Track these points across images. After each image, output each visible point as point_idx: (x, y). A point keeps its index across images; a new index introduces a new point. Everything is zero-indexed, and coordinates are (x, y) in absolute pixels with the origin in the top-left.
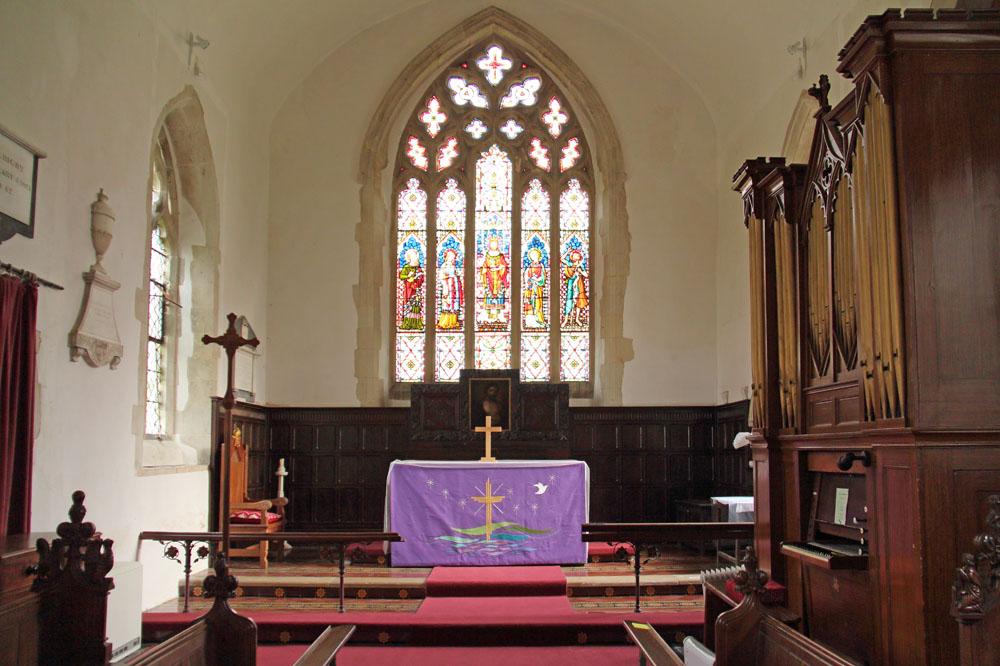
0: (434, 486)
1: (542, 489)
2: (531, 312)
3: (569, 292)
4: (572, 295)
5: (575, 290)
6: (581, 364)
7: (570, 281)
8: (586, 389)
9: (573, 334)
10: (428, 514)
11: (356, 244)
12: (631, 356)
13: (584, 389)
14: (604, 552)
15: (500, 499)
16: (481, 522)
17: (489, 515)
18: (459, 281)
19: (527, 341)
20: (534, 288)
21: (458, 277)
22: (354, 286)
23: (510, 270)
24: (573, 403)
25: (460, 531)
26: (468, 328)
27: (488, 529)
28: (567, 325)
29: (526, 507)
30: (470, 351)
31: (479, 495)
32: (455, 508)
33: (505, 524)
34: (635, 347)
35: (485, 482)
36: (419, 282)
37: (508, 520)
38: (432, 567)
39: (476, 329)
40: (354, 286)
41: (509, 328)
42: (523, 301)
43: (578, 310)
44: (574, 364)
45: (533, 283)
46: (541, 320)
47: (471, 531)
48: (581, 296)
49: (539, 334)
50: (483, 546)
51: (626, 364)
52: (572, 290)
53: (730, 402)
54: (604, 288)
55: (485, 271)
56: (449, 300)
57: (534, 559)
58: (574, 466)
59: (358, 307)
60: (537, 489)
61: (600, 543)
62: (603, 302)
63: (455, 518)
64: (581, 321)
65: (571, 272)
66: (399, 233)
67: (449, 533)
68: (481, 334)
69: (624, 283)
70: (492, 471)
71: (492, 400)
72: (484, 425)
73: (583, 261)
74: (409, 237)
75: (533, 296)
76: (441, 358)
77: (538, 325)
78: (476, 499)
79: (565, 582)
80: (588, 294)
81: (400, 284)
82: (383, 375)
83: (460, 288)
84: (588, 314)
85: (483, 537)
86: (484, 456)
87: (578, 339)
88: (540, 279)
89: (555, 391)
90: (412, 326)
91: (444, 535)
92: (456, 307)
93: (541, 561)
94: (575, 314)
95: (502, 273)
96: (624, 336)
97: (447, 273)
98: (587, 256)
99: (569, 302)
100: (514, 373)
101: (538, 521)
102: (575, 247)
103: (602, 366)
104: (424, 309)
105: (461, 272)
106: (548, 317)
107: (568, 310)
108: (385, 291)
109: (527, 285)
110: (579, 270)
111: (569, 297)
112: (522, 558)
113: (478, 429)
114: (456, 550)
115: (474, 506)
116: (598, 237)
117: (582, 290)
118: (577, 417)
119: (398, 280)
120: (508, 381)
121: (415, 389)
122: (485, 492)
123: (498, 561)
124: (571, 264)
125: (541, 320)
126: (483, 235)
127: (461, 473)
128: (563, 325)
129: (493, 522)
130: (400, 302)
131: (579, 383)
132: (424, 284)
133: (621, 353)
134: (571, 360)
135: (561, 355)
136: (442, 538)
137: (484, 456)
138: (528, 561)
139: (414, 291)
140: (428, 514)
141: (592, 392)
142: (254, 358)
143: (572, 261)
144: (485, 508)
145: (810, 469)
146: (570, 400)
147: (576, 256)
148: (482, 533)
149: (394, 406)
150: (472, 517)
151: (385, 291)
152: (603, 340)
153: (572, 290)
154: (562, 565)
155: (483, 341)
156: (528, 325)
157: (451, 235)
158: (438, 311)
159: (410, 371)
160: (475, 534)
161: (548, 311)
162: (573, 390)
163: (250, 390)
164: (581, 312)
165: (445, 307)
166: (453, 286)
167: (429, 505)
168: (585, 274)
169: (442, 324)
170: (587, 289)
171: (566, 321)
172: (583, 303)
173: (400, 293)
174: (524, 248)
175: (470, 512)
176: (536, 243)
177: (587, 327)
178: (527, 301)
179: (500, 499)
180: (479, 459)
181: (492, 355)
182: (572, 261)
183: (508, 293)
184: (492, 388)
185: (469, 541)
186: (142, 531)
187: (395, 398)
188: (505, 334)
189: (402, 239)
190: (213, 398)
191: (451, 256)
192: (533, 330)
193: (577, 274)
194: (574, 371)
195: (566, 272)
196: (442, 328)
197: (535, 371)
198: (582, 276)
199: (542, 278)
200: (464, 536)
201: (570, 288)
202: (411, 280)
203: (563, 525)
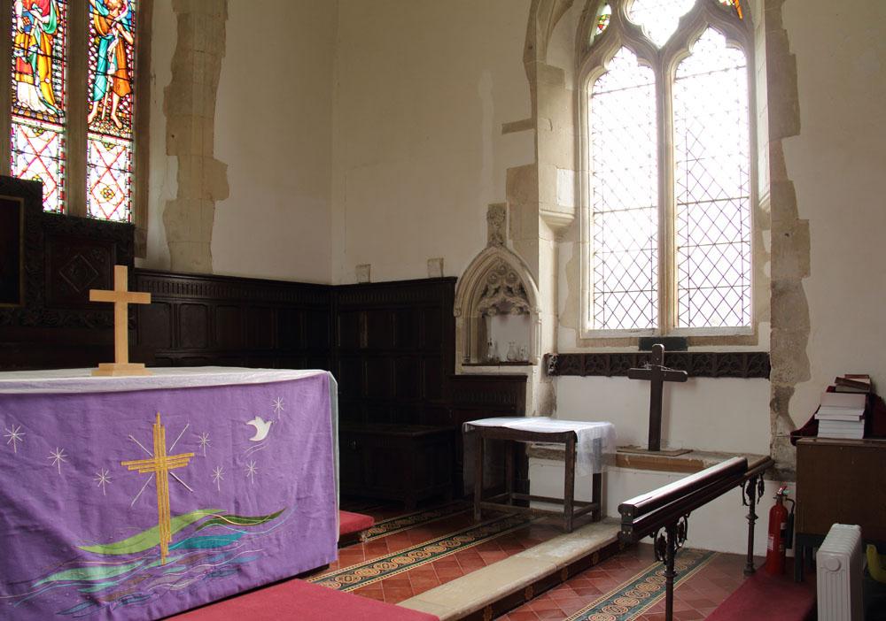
0: (25, 445)
1: (262, 429)
3: (101, 60)
4: (107, 68)
5: (112, 60)
6: (119, 196)
7: (104, 42)
9: (107, 139)
10: (12, 521)
12: (225, 194)
15: (184, 459)
16: (142, 520)
17: (164, 503)
25: (98, 549)
27: (162, 535)
28: (97, 118)
29: (235, 469)
31: (139, 455)
32: (82, 494)
33: (198, 515)
35: (152, 424)
37: (202, 506)
43: (116, 99)
44: (108, 194)
46: (48, 99)
47: (126, 546)
48: (122, 74)
49: (45, 126)
50: (154, 575)
51: (218, 203)
52: (106, 59)
54: (177, 70)
57: (257, 577)
58: (312, 378)
60: (254, 430)
63: (84, 516)
64: (120, 119)
67: (72, 560)
70: (166, 395)
77: (43, 108)
78: (131, 465)
85: (149, 555)
86: (113, 360)
87: (115, 151)
91: (58, 570)
93: (271, 579)
94: (111, 104)
99: (101, 80)
101: (258, 496)
103: (169, 203)
107: (99, 94)
109: (20, 23)
111: (101, 69)
112: (233, 582)
113: (96, 295)
114: (93, 600)
115: (130, 483)
117: (122, 65)
120: (19, 202)
122: (151, 447)
123: (189, 601)
124: (106, 12)
125: (48, 99)
127: (94, 404)
129: (174, 514)
134: (101, 186)
135: (86, 175)
136: (54, 578)
137: (113, 360)
138: (245, 583)
140: (12, 521)
144: (153, 487)
145: (664, 383)
148: (152, 545)
150: (128, 512)
153: (106, 59)
154: (303, 576)
160: (135, 550)
164: (120, 102)
167: (15, 498)
171: (94, 113)
172: (124, 88)
175: (122, 498)
179: (184, 459)
185: (123, 570)
190: (159, 545)
192: (34, 114)
200: (112, 559)
201: (102, 53)
203: (298, 499)
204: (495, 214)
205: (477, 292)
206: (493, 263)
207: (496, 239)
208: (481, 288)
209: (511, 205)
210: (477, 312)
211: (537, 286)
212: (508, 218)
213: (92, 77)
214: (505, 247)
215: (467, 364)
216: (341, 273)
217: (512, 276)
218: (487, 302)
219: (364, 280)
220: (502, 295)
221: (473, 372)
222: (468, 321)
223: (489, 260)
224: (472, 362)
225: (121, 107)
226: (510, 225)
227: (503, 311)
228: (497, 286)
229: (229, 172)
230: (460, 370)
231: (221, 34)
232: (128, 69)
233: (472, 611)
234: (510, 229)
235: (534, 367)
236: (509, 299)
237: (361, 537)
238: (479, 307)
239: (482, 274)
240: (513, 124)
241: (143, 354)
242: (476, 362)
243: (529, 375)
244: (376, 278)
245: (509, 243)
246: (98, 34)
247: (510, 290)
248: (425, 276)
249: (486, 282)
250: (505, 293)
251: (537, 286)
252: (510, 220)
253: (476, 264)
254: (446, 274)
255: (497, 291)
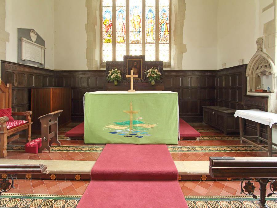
2: (149, 36)
3: (162, 29)
5: (164, 28)
7: (163, 25)
8: (169, 65)
11: (86, 8)
12: (186, 51)
13: (167, 64)
14: (185, 136)
18: (124, 25)
19: (147, 47)
20: (150, 28)
21: (124, 24)
22: (85, 24)
23: (141, 21)
24: (164, 69)
26: (127, 42)
30: (128, 50)
34: (187, 47)
36: (110, 26)
38: (106, 144)
39: (130, 43)
40: (85, 24)
41: (141, 43)
42: (146, 33)
43: (165, 36)
45: (150, 26)
48: (166, 30)
51: (183, 54)
53: (226, 68)
54: (175, 26)
55: (133, 21)
56: (121, 32)
59: (87, 32)
61: (99, 17)
62: (175, 31)
65: (163, 22)
66: (103, 7)
68: (131, 44)
69: (183, 23)
71: (135, 67)
72: (130, 75)
73: (167, 18)
74: (107, 9)
75: (150, 31)
76: (117, 53)
77: (151, 42)
79: (177, 171)
80: (168, 30)
81: (104, 26)
82: (97, 58)
83: (124, 28)
84: (168, 37)
86: (130, 89)
88: (152, 24)
89: (158, 64)
90: (108, 42)
92: (123, 35)
95: (139, 22)
96: (183, 43)
97: (120, 24)
98: (168, 16)
100: (143, 57)
102: (164, 11)
104: (112, 35)
105: (125, 22)
106: (155, 38)
107: (162, 36)
108: (97, 27)
110: (166, 21)
111: (162, 31)
116: (173, 7)
117: (166, 28)
118: (166, 73)
119: (103, 25)
121: (108, 64)
126: (132, 9)
128: (160, 42)
130: (104, 33)
131: (166, 63)
132: (112, 26)
133: (182, 50)
137: (130, 89)
139: (108, 29)
141: (170, 65)
142: (41, 49)
143: (163, 17)
146: (9, 84)
147: (164, 16)
149: (101, 70)
151: (97, 27)
152: (175, 45)
155: (132, 47)
156: (148, 41)
157: (121, 8)
158: (117, 36)
159: (107, 57)
161: (155, 36)
162: (164, 64)
163: (40, 62)
164: (166, 36)
165: (119, 35)
166: (122, 27)
168: (168, 22)
169: (118, 41)
170: (168, 28)
173: (104, 30)
174: (146, 13)
176: (151, 11)
177: (168, 42)
178: (147, 32)
180: (127, 90)
181: (135, 51)
182: (163, 17)
183: (141, 30)
184: (135, 63)
186: (186, 53)
187: (102, 68)
188: (139, 44)
189: (104, 9)
191: (121, 16)
193: (165, 22)
194: (164, 58)
195: (161, 22)
196: (118, 42)
197: (150, 57)
198: (167, 23)
199: (153, 24)
201: (162, 27)
202: (107, 25)
204: (260, 42)
205: (255, 68)
206: (259, 58)
207: (260, 49)
208: (256, 66)
209: (265, 37)
210: (255, 75)
211: (274, 64)
212: (264, 41)
213: (160, 33)
214: (263, 52)
215: (251, 92)
216: (219, 67)
217: (267, 61)
218: (258, 71)
219: (224, 68)
220: (263, 68)
221: (258, 94)
222: (252, 78)
223: (258, 57)
224: (253, 91)
225: (166, 37)
226: (265, 44)
227: (263, 73)
228: (261, 65)
229: (187, 46)
230: (248, 94)
231: (184, 14)
232: (168, 29)
233: (194, 174)
234: (265, 45)
235: (271, 94)
236: (266, 70)
237: (197, 139)
238: (256, 73)
239: (257, 60)
240: (265, 8)
241: (135, 88)
242: (254, 91)
243: (269, 96)
244: (227, 66)
245: (264, 50)
246: (161, 24)
247: (266, 66)
248: (239, 65)
249: (258, 65)
250: (264, 68)
251: (274, 64)
252: (265, 42)
253: (253, 59)
254: (244, 63)
255: (261, 67)
